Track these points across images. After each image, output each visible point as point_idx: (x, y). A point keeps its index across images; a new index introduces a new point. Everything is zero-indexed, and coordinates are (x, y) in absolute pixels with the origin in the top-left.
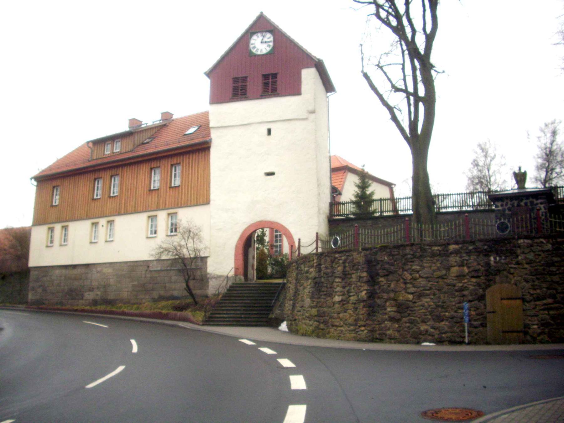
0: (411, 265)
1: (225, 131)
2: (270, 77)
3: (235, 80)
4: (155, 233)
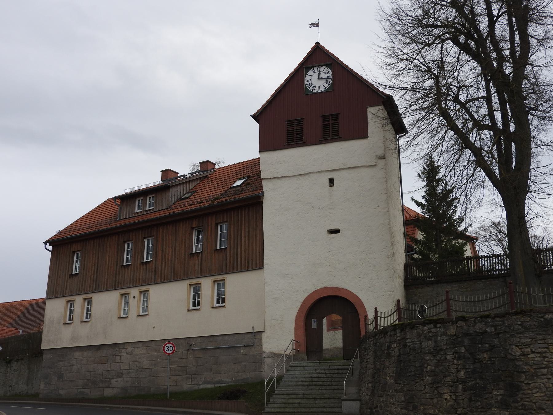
0: (519, 338)
1: (278, 182)
2: (330, 117)
3: (290, 123)
4: (223, 301)
